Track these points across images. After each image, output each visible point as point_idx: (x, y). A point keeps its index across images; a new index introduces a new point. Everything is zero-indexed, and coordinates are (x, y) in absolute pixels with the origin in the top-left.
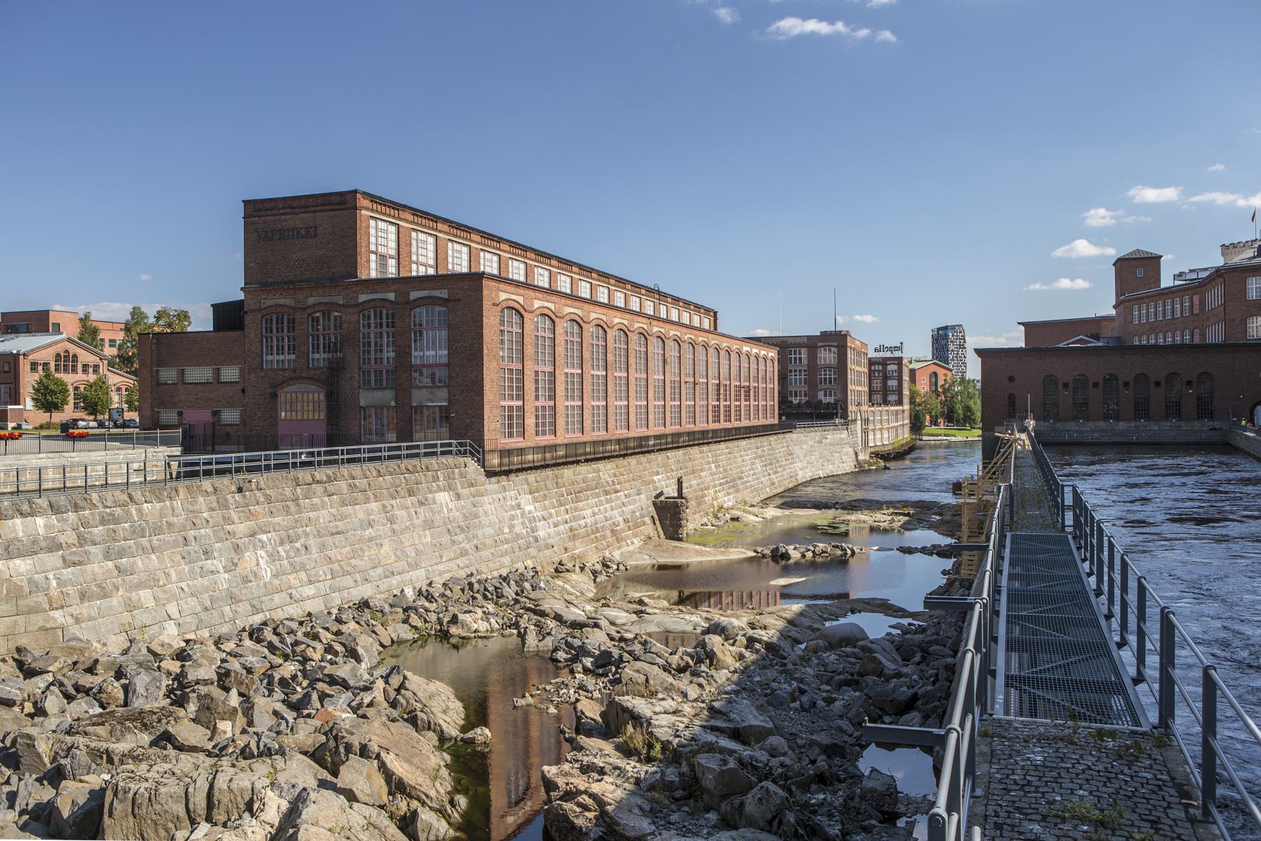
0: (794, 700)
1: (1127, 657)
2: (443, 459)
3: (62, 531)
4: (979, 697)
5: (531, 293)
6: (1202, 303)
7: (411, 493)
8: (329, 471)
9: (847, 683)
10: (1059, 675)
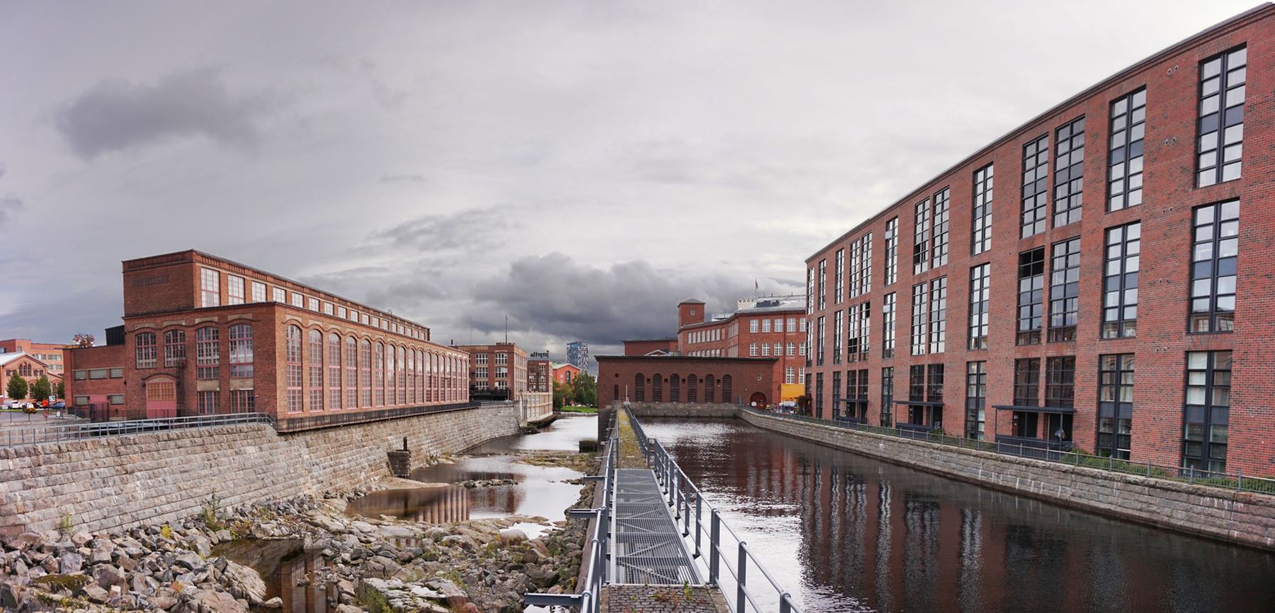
0: (481, 579)
1: (689, 543)
2: (251, 424)
4: (601, 571)
6: (727, 334)
7: (230, 447)
8: (178, 431)
9: (515, 568)
10: (650, 556)
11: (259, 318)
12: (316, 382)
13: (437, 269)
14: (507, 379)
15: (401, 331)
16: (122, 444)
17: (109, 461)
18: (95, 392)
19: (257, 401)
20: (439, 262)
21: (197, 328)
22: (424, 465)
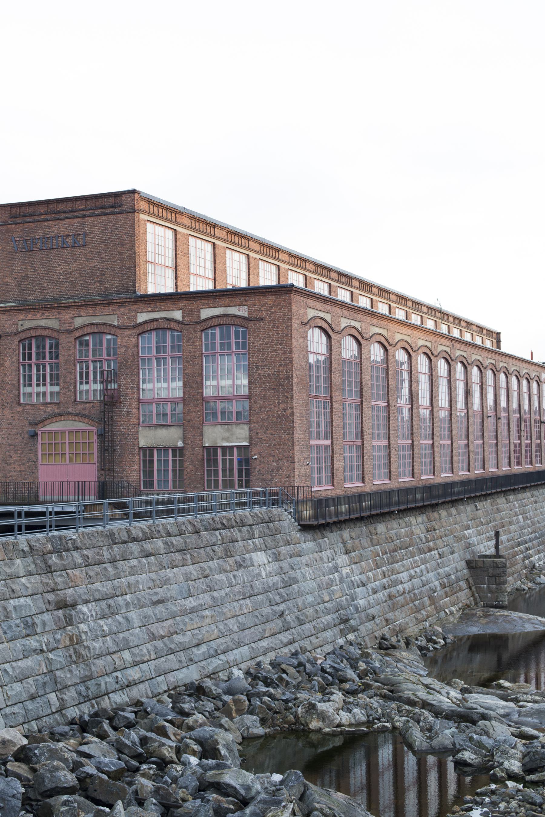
2: (257, 510)
19: (257, 468)
21: (143, 329)
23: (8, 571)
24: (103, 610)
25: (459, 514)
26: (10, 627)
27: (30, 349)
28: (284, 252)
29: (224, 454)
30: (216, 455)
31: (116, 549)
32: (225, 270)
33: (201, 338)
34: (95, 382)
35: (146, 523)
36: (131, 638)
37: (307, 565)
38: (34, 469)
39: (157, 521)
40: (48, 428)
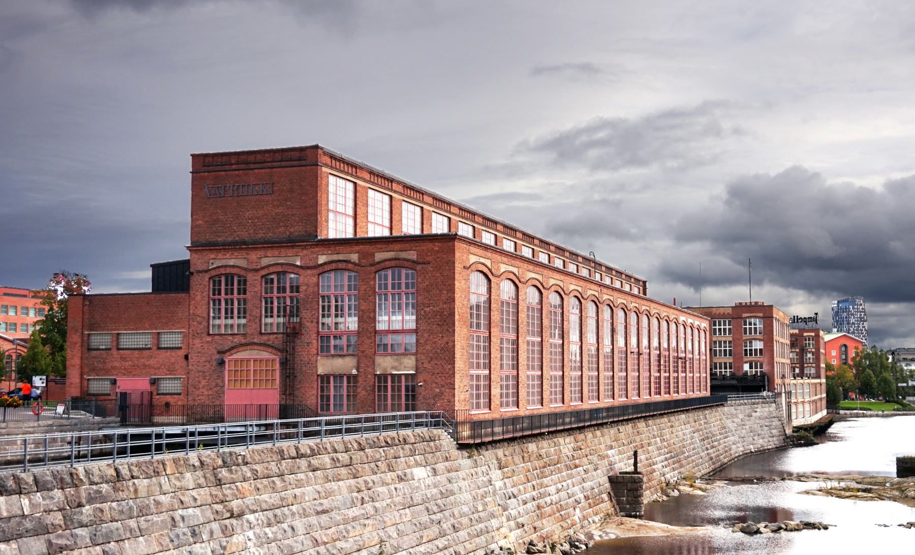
2: (418, 430)
3: (48, 511)
5: (498, 257)
7: (391, 468)
11: (427, 263)
12: (508, 362)
13: (618, 196)
14: (764, 359)
15: (627, 288)
16: (225, 464)
17: (203, 494)
18: (128, 372)
19: (422, 393)
20: (621, 187)
22: (657, 496)
23: (178, 484)
24: (269, 519)
25: (603, 436)
26: (178, 536)
27: (220, 284)
28: (454, 205)
29: (393, 382)
30: (386, 381)
31: (284, 464)
32: (401, 220)
33: (375, 278)
34: (279, 316)
35: (313, 441)
36: (295, 545)
37: (464, 479)
38: (220, 394)
39: (324, 440)
40: (235, 356)
